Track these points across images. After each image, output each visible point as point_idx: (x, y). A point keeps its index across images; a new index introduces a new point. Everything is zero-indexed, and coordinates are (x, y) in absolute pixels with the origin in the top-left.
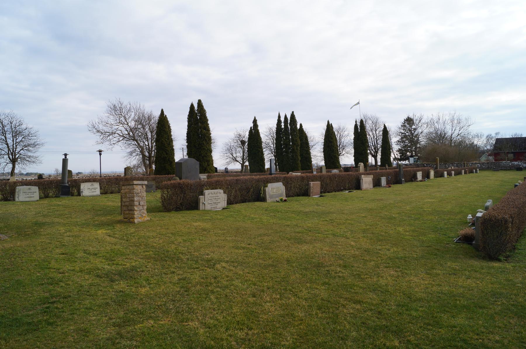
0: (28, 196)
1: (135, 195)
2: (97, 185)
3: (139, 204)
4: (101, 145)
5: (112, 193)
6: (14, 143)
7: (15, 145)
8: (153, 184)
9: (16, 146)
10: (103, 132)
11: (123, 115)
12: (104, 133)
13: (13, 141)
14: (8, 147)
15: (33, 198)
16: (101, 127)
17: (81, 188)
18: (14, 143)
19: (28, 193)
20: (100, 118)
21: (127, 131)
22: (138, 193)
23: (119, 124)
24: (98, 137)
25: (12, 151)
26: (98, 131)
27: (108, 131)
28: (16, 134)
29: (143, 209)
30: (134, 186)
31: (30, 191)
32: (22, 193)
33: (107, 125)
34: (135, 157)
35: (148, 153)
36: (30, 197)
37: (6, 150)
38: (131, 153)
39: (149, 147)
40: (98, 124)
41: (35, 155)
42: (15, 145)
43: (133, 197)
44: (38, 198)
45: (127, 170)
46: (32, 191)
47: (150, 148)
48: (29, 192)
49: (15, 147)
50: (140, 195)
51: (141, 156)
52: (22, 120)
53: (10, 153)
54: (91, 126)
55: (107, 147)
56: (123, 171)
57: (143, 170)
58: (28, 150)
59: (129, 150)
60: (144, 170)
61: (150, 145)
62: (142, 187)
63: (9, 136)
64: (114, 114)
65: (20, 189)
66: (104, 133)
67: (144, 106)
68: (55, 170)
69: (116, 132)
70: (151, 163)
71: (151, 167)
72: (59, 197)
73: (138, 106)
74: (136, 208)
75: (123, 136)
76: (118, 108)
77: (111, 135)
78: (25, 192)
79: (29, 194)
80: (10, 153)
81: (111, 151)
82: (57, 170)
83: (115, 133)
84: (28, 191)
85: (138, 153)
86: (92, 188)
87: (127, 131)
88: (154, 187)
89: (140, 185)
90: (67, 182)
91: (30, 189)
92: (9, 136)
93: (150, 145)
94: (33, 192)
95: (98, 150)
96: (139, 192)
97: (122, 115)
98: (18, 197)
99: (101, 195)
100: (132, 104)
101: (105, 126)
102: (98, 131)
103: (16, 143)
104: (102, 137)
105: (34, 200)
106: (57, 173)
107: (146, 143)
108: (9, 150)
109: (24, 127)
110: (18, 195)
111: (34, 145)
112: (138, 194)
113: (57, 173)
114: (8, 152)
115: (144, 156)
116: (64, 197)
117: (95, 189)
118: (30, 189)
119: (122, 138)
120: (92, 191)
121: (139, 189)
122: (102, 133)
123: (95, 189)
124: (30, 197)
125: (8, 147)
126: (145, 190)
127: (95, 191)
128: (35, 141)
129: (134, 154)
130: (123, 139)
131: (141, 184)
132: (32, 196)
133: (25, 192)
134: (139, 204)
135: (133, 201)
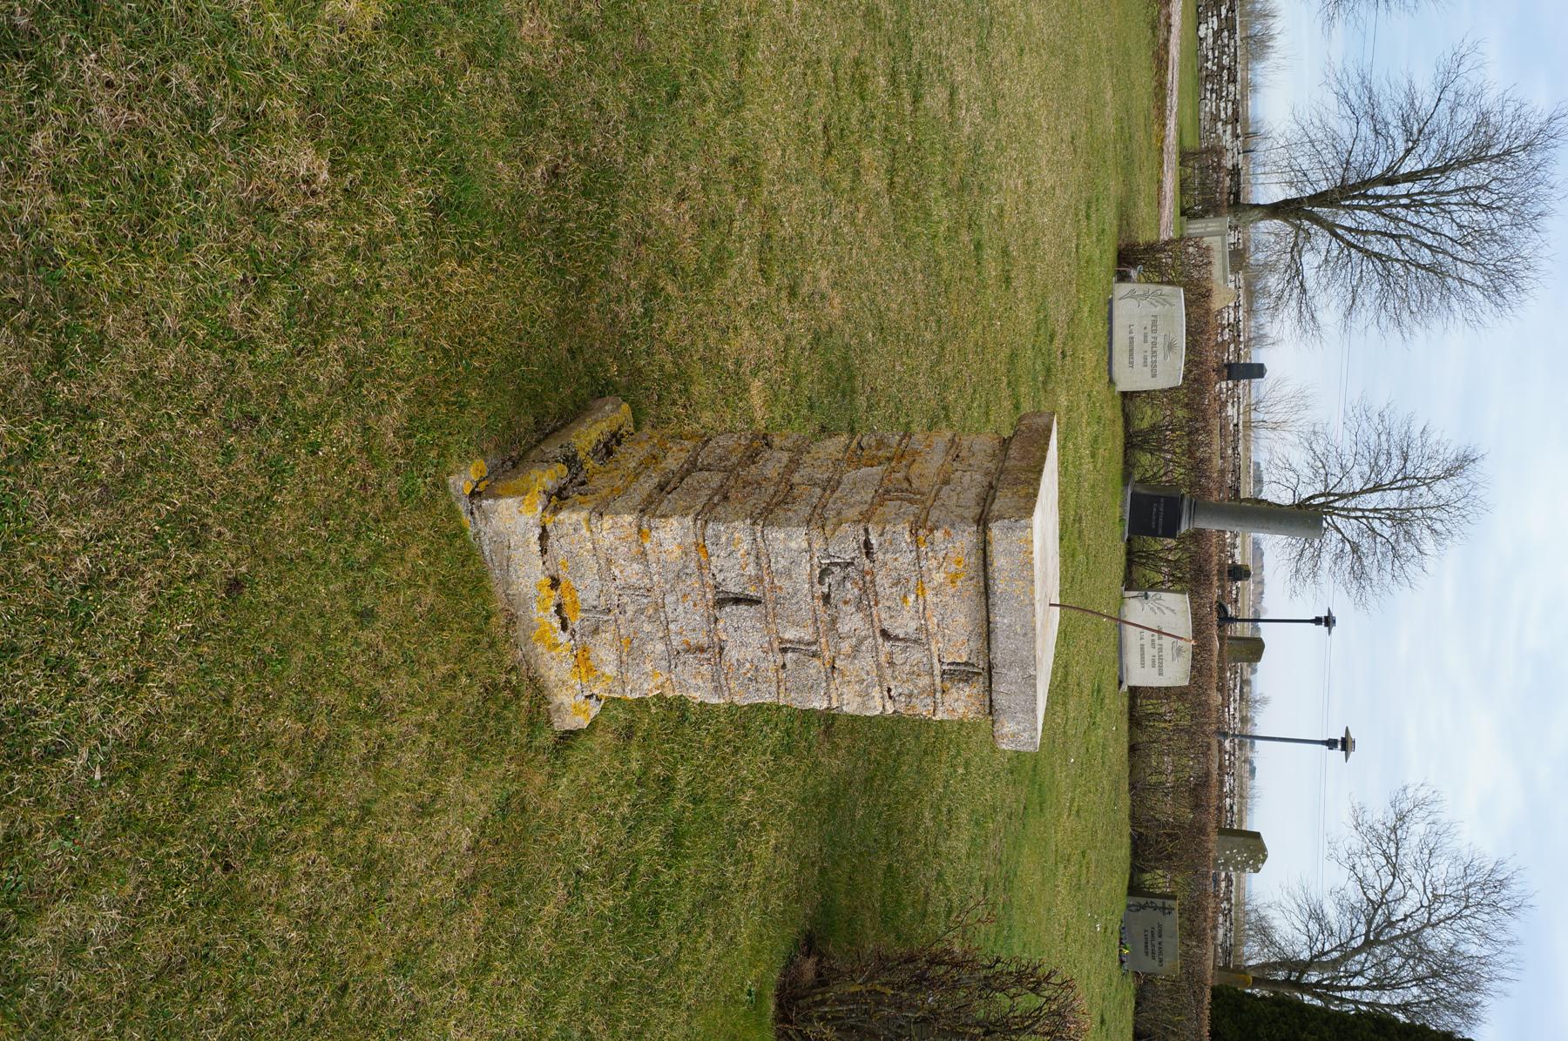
0: (1138, 339)
1: (846, 546)
2: (1175, 673)
3: (726, 600)
4: (1352, 823)
5: (1133, 749)
6: (1367, 513)
7: (1359, 514)
8: (1166, 964)
9: (1356, 518)
10: (1399, 832)
11: (1467, 912)
12: (1393, 837)
13: (1375, 510)
14: (1354, 494)
15: (1127, 361)
16: (1416, 831)
17: (1164, 595)
18: (1367, 513)
19: (1150, 339)
20: (1453, 830)
21: (1404, 920)
22: (867, 599)
23: (1430, 895)
24: (1379, 816)
25: (1336, 505)
26: (1401, 818)
27: (1401, 852)
28: (1399, 518)
29: (674, 656)
30: (966, 538)
31: (1160, 348)
32: (1155, 311)
33: (1426, 851)
34: (1302, 928)
35: (1318, 984)
36: (1131, 350)
37: (1345, 487)
38: (1317, 916)
39: (1341, 989)
40: (1430, 819)
41: (1324, 575)
42: (1359, 514)
43: (817, 519)
44: (1124, 385)
45: (1250, 841)
46: (1160, 357)
47: (1338, 994)
48: (1154, 344)
49: (1353, 514)
50: (852, 622)
51: (1305, 955)
52: (1456, 538)
53: (1332, 498)
54: (1421, 794)
55: (1340, 844)
56: (1252, 825)
57: (1249, 959)
58: (1340, 556)
59: (1332, 913)
60: (1251, 963)
61: (1348, 995)
62: (959, 674)
63: (1391, 499)
64: (1470, 880)
65: (1174, 301)
66: (1393, 837)
67: (1506, 995)
68: (1266, 695)
69: (1397, 880)
70: (1276, 989)
71: (1257, 982)
72: (1125, 484)
73: (1506, 973)
74: (672, 534)
75: (1382, 903)
76: (1494, 897)
77: (1388, 858)
78: (1154, 323)
79: (1148, 347)
80: (1332, 498)
81: (1326, 854)
82: (1265, 613)
83: (1394, 875)
84: (1160, 340)
85: (1319, 945)
86: (1160, 650)
87: (1404, 920)
88: (1150, 965)
89: (987, 633)
90: (1201, 524)
91: (1171, 346)
92: (1391, 499)
93: (1348, 995)
94: (1154, 363)
95: (1353, 735)
96: (881, 612)
97: (1466, 907)
98: (1132, 295)
99: (1125, 688)
100: (1512, 949)
101: (1424, 843)
102: (1401, 818)
103: (1367, 518)
104: (1379, 827)
105: (1116, 369)
106: (1256, 702)
107: (1359, 981)
108: (1342, 496)
109: (1428, 544)
110: (1145, 296)
111: (1359, 574)
112: (852, 591)
113: (1256, 702)
114: (1335, 495)
115: (1305, 966)
116: (1123, 506)
117: (1159, 664)
118: (1171, 346)
119: (1373, 897)
120: (1148, 649)
121: (922, 614)
122: (1394, 830)
123: (1159, 664)
124: (1131, 350)
125: (1354, 494)
126: (922, 708)
127: (1148, 662)
128: (1374, 583)
129: (1314, 927)
130: (1372, 902)
131: (999, 656)
132: (1138, 359)
133: (1154, 323)
134: (726, 600)
135: (766, 515)
